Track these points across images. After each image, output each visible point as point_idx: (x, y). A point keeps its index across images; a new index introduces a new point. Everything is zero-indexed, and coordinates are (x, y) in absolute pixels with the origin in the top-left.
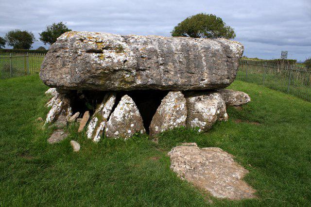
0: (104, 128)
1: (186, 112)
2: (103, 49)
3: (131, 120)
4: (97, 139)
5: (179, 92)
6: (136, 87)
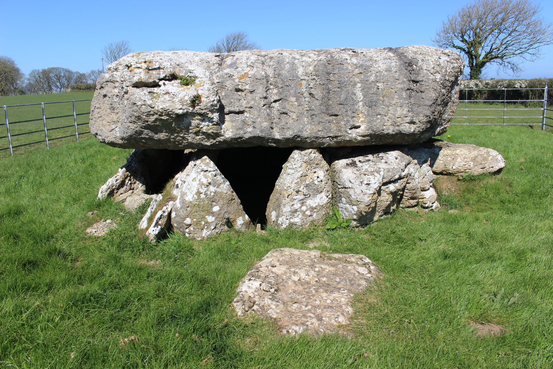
0: (170, 214)
1: (329, 187)
6: (225, 141)
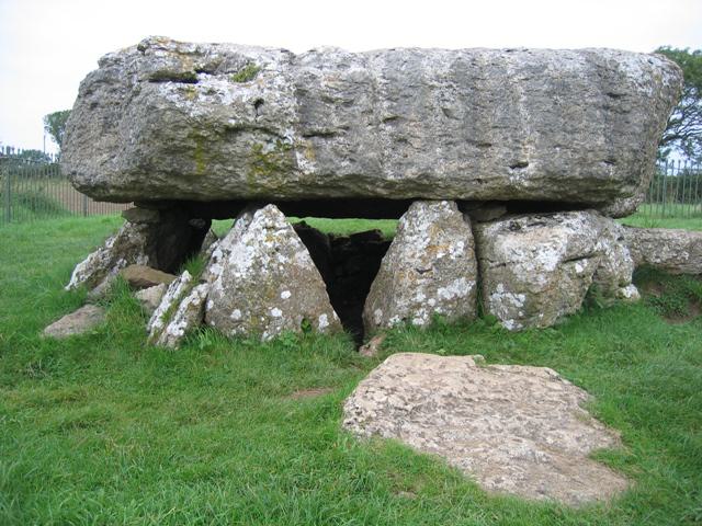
0: (204, 303)
1: (472, 267)
2: (199, 71)
3: (278, 279)
4: (176, 329)
5: (444, 203)
6: (302, 183)
